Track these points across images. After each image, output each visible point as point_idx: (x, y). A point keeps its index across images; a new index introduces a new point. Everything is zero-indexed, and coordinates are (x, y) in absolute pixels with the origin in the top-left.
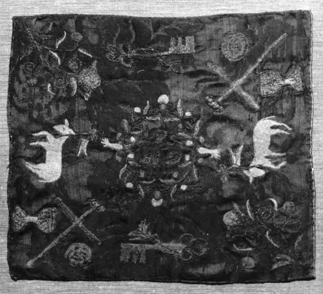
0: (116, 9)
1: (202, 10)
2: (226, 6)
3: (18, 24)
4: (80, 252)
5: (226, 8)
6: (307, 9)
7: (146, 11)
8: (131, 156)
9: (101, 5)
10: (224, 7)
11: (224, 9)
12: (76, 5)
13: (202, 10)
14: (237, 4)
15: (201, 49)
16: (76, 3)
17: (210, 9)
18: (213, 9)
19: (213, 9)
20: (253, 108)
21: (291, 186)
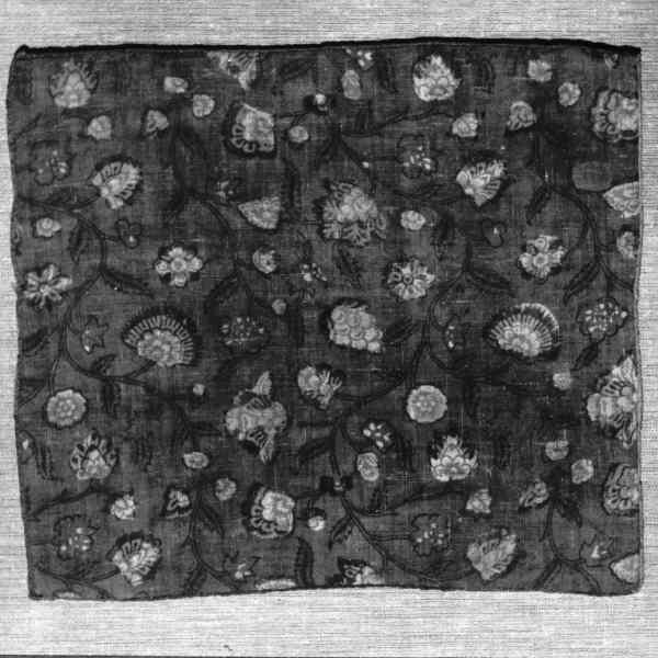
0: (427, 620)
1: (252, 618)
2: (204, 628)
3: (528, 435)
4: (432, 83)
5: (204, 624)
6: (41, 608)
7: (367, 617)
8: (370, 469)
9: (458, 628)
10: (210, 624)
11: (207, 620)
12: (510, 627)
13: (252, 618)
14: (180, 630)
15: (565, 11)
16: (510, 631)
17: (237, 620)
18: (229, 622)
19: (229, 622)
20: (77, 587)
21: (631, 141)
